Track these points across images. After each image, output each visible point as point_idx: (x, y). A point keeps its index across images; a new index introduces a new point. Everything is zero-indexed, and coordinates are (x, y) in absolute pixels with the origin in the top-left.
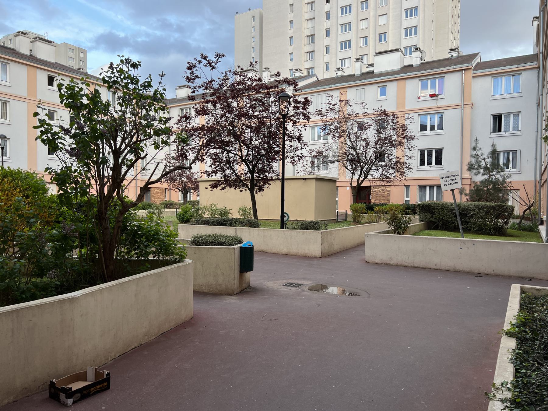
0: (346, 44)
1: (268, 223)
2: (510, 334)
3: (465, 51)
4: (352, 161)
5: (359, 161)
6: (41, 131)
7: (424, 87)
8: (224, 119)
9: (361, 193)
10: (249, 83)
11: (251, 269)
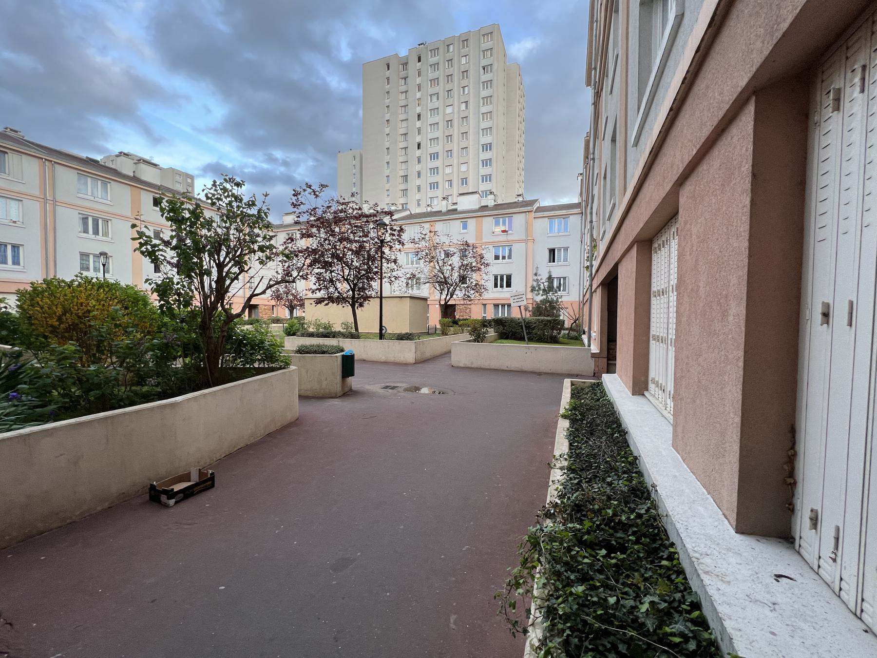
0: (434, 185)
1: (368, 336)
2: (565, 417)
3: (528, 198)
4: (440, 283)
5: (446, 283)
6: (140, 243)
7: (497, 224)
8: (327, 242)
9: (448, 310)
10: (350, 211)
11: (353, 375)
